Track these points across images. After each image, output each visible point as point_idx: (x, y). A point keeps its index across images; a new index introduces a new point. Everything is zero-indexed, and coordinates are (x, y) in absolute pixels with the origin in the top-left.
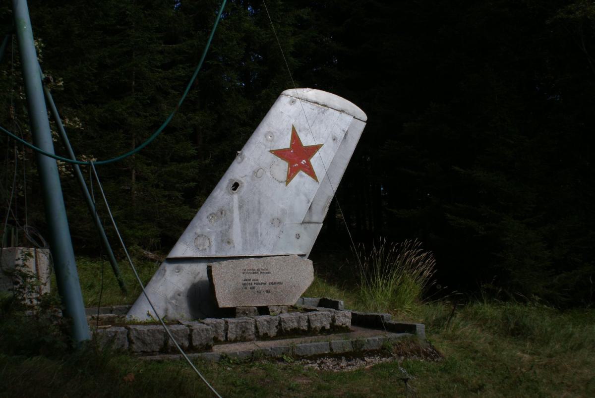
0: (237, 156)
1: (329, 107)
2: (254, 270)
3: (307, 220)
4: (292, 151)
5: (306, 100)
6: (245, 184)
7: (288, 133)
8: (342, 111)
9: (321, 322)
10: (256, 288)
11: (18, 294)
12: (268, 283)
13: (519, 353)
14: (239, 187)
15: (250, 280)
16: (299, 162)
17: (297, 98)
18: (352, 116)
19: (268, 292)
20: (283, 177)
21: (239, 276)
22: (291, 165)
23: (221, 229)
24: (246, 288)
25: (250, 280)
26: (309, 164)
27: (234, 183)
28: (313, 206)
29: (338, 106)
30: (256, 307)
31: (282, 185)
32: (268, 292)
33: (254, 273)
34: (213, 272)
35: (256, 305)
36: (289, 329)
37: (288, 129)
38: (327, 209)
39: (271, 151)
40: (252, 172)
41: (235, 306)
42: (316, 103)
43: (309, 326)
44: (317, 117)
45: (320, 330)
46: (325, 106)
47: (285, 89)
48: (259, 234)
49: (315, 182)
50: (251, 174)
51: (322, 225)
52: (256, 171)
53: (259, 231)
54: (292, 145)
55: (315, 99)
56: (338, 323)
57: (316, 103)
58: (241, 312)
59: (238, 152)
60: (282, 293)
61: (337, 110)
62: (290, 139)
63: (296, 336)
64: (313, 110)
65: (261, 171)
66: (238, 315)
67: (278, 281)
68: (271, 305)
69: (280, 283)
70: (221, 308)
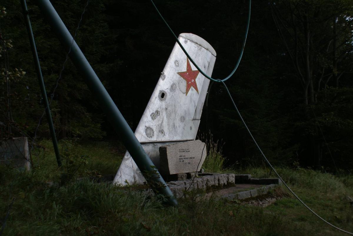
0: (161, 76)
1: (202, 46)
2: (183, 150)
3: (194, 118)
4: (188, 74)
5: (192, 41)
6: (168, 94)
7: (185, 62)
8: (207, 49)
9: (223, 181)
10: (184, 161)
11: (133, 199)
12: (189, 158)
13: (33, 143)
14: (164, 96)
15: (182, 156)
16: (191, 81)
17: (188, 39)
18: (211, 52)
19: (189, 163)
20: (184, 90)
21: (178, 154)
22: (188, 83)
23: (158, 124)
24: (180, 162)
25: (182, 156)
26: (195, 82)
27: (162, 93)
28: (197, 108)
29: (206, 47)
30: (186, 173)
31: (185, 95)
32: (189, 163)
33: (183, 152)
34: (167, 151)
35: (186, 172)
36: (210, 186)
37: (185, 59)
38: (202, 111)
39: (178, 73)
40: (170, 86)
41: (176, 173)
42: (196, 43)
43: (219, 184)
44: (197, 52)
45: (223, 186)
46: (200, 45)
47: (179, 34)
48: (176, 127)
49: (198, 94)
50: (170, 87)
51: (200, 121)
52: (172, 86)
53: (176, 125)
54: (188, 70)
55: (196, 41)
56: (230, 181)
57: (196, 43)
58: (180, 176)
59: (162, 73)
60: (195, 164)
61: (206, 49)
62: (186, 65)
63: (118, 168)
64: (196, 47)
65: (174, 85)
66: (179, 179)
67: (193, 156)
68: (191, 172)
69: (194, 158)
70: (171, 175)
